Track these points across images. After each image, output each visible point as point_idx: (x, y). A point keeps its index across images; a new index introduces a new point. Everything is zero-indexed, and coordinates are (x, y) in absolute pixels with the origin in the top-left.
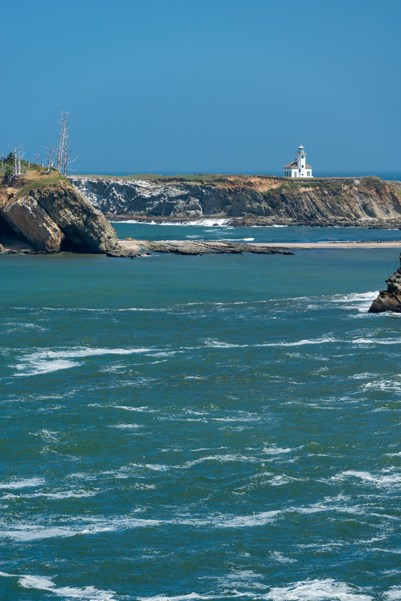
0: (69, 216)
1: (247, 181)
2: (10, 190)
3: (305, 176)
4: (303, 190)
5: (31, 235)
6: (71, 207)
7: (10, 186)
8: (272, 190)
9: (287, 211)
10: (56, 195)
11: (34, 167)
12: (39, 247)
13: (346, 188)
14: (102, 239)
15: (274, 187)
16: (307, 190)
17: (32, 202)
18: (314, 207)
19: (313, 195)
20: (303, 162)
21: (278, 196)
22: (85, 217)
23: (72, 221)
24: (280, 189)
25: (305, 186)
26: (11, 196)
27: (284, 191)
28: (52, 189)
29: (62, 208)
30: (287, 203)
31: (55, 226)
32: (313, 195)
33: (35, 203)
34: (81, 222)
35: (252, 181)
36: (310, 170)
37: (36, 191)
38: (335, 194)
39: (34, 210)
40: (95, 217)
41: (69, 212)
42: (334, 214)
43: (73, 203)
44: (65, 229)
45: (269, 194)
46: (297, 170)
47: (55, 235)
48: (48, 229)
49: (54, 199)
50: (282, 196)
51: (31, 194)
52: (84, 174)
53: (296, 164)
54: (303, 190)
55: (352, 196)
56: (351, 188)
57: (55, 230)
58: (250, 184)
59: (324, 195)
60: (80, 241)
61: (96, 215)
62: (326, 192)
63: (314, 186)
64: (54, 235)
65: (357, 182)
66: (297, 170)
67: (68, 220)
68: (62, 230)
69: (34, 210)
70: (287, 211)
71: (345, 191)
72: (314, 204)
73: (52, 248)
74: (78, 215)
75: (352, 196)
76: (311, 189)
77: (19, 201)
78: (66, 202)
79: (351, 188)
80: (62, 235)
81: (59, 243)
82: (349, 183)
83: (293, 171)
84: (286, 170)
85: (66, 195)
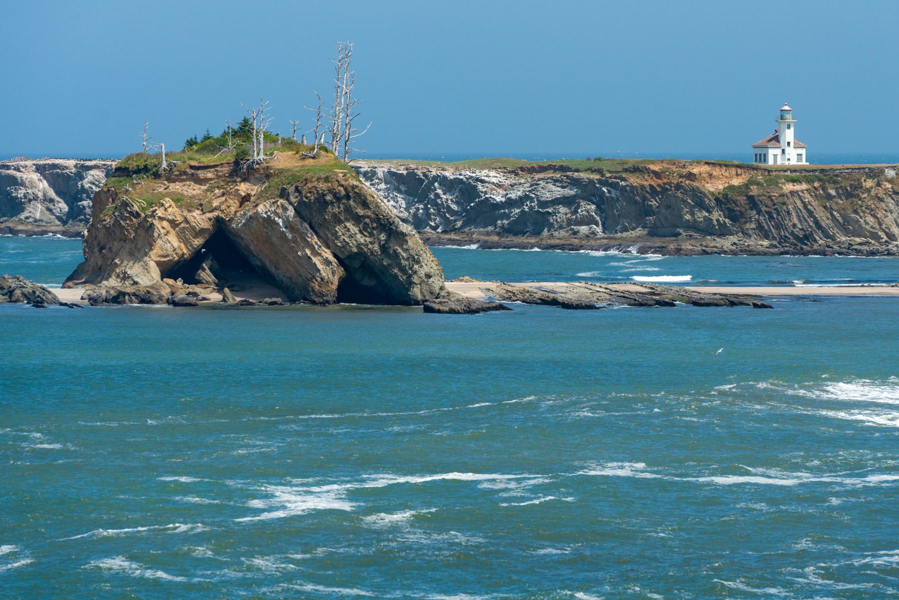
0: (353, 236)
1: (685, 171)
2: (243, 188)
3: (794, 162)
4: (789, 187)
5: (283, 272)
6: (357, 219)
7: (244, 180)
8: (731, 188)
9: (760, 227)
10: (329, 198)
11: (289, 144)
12: (297, 291)
13: (869, 183)
14: (415, 279)
15: (736, 182)
16: (797, 187)
17: (285, 209)
18: (811, 221)
19: (808, 198)
20: (789, 135)
21: (742, 199)
22: (383, 237)
23: (359, 246)
24: (747, 186)
25: (794, 181)
26: (245, 199)
27: (754, 191)
28: (323, 186)
29: (340, 222)
30: (759, 212)
31: (328, 254)
32: (808, 198)
33: (291, 212)
34: (376, 247)
35: (695, 171)
36: (803, 151)
37: (291, 189)
38: (849, 195)
39: (288, 225)
40: (402, 237)
41: (354, 229)
42: (846, 232)
43: (360, 211)
44: (344, 259)
45: (725, 196)
46: (778, 152)
47: (327, 270)
48: (315, 260)
49: (326, 204)
50: (751, 199)
51: (284, 194)
52: (382, 158)
53: (776, 139)
54: (789, 187)
55: (881, 200)
56: (879, 185)
57: (327, 262)
58: (691, 176)
59: (829, 197)
60: (373, 284)
61: (404, 235)
62: (833, 192)
63: (809, 181)
64: (325, 271)
65: (890, 173)
66: (778, 152)
67: (352, 243)
68: (341, 262)
69: (288, 225)
70: (760, 227)
71: (868, 190)
72: (811, 214)
73: (321, 295)
74: (371, 235)
75: (881, 200)
76: (804, 186)
77: (261, 209)
78: (348, 210)
79: (879, 185)
80: (340, 272)
81: (335, 287)
82: (876, 174)
83: (771, 152)
84: (759, 151)
85: (348, 197)
